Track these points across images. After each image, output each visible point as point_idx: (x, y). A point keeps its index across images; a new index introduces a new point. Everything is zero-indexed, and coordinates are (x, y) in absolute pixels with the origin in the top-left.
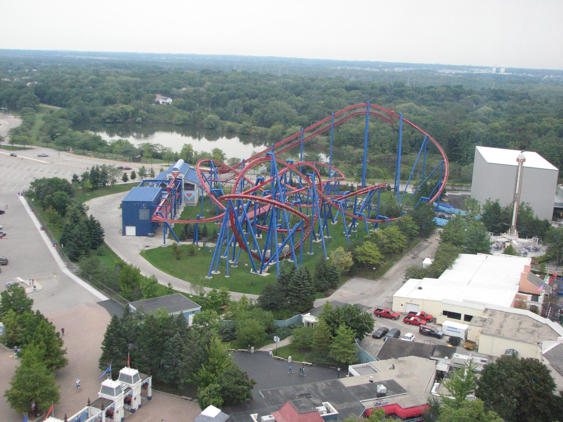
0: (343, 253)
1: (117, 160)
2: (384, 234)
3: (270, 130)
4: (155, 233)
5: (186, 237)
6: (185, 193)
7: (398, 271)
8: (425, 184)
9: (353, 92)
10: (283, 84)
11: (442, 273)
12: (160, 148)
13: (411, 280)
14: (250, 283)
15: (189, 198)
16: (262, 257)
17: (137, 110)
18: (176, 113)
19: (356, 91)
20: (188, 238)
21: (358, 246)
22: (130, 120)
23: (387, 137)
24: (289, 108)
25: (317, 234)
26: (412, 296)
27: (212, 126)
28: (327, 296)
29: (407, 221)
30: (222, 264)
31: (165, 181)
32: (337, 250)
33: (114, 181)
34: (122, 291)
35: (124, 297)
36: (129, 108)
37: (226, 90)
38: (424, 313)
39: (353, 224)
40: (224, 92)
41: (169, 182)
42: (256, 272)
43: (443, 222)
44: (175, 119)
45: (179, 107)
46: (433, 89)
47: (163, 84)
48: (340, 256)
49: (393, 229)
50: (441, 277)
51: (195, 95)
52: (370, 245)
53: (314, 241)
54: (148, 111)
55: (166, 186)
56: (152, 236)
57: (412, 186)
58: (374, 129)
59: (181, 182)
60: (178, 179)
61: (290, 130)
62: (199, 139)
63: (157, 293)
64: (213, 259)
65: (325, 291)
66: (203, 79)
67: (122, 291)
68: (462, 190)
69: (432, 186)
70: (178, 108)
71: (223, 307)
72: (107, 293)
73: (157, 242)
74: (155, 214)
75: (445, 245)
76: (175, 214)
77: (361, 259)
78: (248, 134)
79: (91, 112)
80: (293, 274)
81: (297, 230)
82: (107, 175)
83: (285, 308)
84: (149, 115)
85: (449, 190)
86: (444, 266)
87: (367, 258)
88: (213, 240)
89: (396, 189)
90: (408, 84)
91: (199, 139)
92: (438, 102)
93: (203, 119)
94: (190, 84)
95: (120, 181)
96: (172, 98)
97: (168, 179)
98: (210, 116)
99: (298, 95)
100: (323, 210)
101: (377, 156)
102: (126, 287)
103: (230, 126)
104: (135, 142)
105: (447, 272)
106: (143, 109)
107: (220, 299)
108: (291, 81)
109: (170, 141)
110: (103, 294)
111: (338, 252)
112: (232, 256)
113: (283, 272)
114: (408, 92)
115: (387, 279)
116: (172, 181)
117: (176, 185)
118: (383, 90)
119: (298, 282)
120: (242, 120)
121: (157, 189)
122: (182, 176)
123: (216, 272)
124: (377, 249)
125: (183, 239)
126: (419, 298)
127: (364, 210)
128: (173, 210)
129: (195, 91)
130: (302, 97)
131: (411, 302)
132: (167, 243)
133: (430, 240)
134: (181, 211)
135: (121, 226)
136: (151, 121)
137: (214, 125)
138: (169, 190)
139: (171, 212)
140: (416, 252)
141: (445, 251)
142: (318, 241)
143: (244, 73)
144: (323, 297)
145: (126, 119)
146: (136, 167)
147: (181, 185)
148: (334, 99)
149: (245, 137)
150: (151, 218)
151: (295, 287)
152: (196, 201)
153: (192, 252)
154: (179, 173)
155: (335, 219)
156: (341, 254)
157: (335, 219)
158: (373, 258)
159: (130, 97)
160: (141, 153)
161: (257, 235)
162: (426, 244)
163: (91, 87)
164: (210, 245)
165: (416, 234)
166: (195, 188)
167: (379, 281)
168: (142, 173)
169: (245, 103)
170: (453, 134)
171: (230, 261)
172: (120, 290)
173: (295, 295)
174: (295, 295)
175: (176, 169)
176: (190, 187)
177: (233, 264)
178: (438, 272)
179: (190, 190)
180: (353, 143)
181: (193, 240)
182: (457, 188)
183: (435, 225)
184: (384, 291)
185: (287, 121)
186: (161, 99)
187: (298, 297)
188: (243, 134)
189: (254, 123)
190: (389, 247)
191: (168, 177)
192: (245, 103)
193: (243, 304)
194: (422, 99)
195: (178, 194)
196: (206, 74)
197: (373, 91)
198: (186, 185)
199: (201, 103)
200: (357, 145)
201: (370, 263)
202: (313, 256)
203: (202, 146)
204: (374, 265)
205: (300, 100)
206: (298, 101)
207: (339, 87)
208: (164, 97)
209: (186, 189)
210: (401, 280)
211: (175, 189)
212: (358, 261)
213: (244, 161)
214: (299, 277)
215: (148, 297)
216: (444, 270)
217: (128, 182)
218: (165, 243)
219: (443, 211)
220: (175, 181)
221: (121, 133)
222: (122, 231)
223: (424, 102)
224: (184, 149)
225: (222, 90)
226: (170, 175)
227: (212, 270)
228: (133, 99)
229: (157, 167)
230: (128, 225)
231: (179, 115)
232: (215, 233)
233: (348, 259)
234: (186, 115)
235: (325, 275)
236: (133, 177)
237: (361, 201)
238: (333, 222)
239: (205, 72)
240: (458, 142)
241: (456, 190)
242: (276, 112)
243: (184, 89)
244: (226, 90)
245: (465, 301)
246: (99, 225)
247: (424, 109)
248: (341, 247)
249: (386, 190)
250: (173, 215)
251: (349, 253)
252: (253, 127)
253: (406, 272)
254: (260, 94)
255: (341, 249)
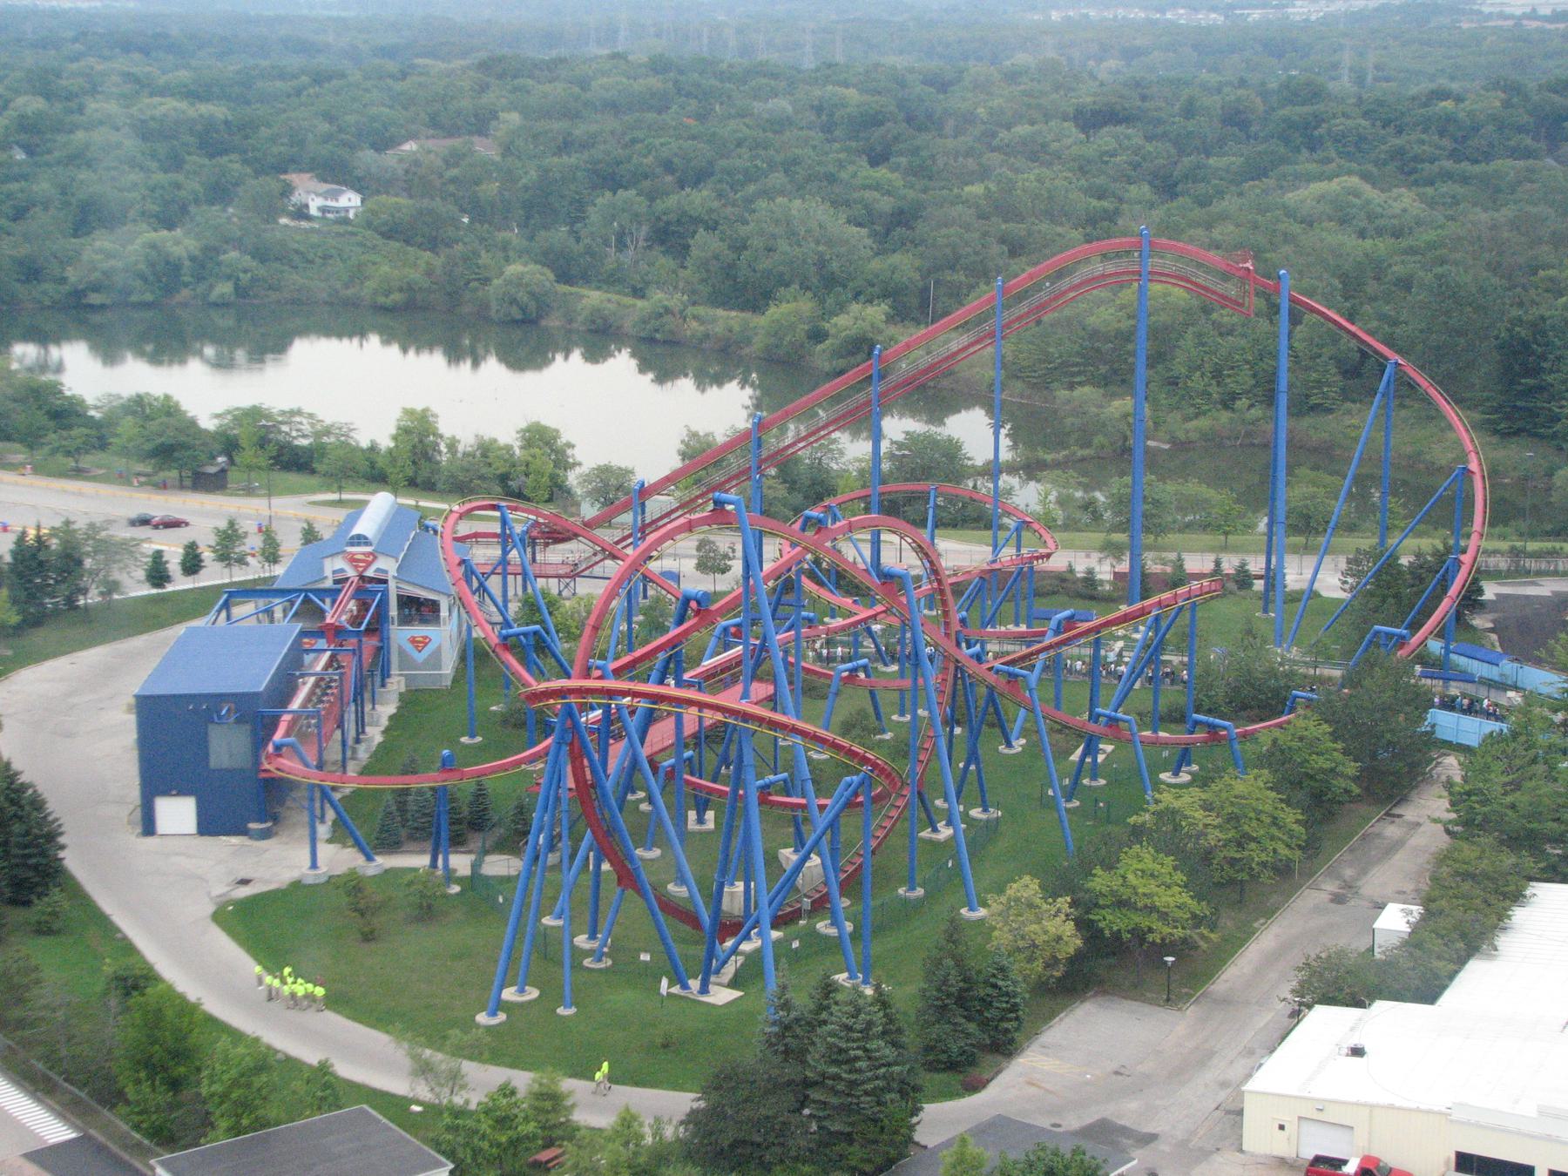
0: (1038, 901)
1: (130, 484)
2: (1207, 807)
3: (761, 321)
4: (275, 819)
5: (403, 832)
6: (400, 635)
7: (1270, 959)
8: (1391, 562)
9: (1106, 138)
10: (819, 110)
11: (1452, 976)
12: (307, 428)
13: (1320, 1010)
14: (659, 1041)
15: (420, 657)
16: (706, 918)
17: (211, 252)
18: (374, 258)
19: (1120, 129)
20: (411, 838)
21: (1098, 871)
22: (185, 293)
23: (1243, 342)
24: (837, 224)
25: (939, 803)
26: (1321, 1090)
27: (523, 309)
28: (974, 1087)
29: (1312, 745)
30: (546, 956)
31: (317, 592)
32: (1013, 890)
33: (113, 587)
34: (127, 1102)
35: (137, 1127)
36: (181, 243)
37: (584, 146)
38: (1376, 1161)
39: (1091, 750)
40: (572, 160)
41: (333, 593)
42: (685, 987)
43: (1471, 730)
44: (370, 285)
45: (390, 233)
46: (1448, 105)
47: (325, 127)
48: (1020, 917)
49: (1250, 787)
50: (1448, 998)
51: (455, 172)
52: (1149, 864)
53: (926, 834)
54: (261, 255)
55: (321, 613)
56: (265, 835)
57: (1343, 565)
58: (1187, 311)
59: (385, 593)
60: (371, 580)
61: (842, 320)
62: (476, 364)
63: (272, 1113)
64: (509, 929)
65: (963, 1068)
66: (488, 98)
67: (127, 1102)
68: (1556, 573)
69: (1420, 572)
70: (383, 234)
71: (544, 1156)
72: (68, 1110)
73: (285, 860)
74: (270, 748)
75: (1468, 851)
76: (361, 724)
77: (1111, 921)
78: (673, 343)
79: (21, 263)
80: (824, 1015)
81: (850, 804)
82: (80, 563)
83: (796, 1159)
84: (262, 272)
85: (1496, 575)
86: (1460, 945)
87: (1137, 919)
88: (511, 843)
89: (1272, 577)
90: (1344, 84)
91: (476, 364)
92: (1465, 166)
93: (486, 281)
94: (434, 123)
95: (137, 588)
96: (358, 191)
97: (329, 584)
98: (514, 269)
99: (875, 162)
100: (960, 700)
101: (1203, 423)
102: (146, 1087)
103: (596, 311)
104: (203, 391)
105: (1475, 970)
106: (238, 244)
107: (531, 1127)
108: (852, 94)
109: (348, 384)
110: (51, 1109)
111: (1017, 900)
112: (587, 917)
113: (786, 1006)
114: (1339, 124)
115: (1225, 1001)
116: (348, 591)
117: (364, 606)
118: (1236, 119)
119: (841, 1051)
120: (647, 283)
121: (287, 629)
122: (387, 565)
123: (522, 991)
124: (1180, 877)
125: (389, 843)
126: (1354, 1100)
127: (1137, 686)
128: (350, 717)
129: (453, 159)
130: (893, 170)
131: (1318, 1115)
132: (323, 868)
133: (1409, 813)
134: (386, 709)
135: (134, 794)
136: (274, 296)
137: (532, 305)
138: (336, 632)
139: (340, 725)
140: (1348, 872)
141: (1466, 876)
142: (945, 832)
143: (659, 66)
144: (959, 1095)
145: (169, 290)
146: (204, 513)
147: (383, 604)
148: (1030, 178)
149: (663, 354)
150: (257, 762)
151: (833, 1070)
152: (448, 667)
153: (427, 906)
154: (374, 556)
155: (1017, 727)
156: (1031, 906)
157: (1017, 727)
158: (1164, 916)
159: (183, 193)
160: (230, 446)
161: (692, 815)
162: (1392, 831)
163: (20, 156)
164: (499, 865)
165: (1347, 791)
166: (444, 613)
167: (1192, 1011)
168: (228, 544)
169: (660, 205)
170: (1520, 321)
171: (581, 940)
172: (121, 1095)
173: (835, 1101)
174: (835, 1101)
175: (360, 540)
176: (419, 609)
177: (590, 953)
178: (1436, 977)
179: (424, 621)
180: (1103, 369)
181: (429, 845)
182: (1531, 564)
183: (1434, 744)
184: (1211, 1054)
185: (831, 283)
186: (313, 197)
187: (846, 1109)
188: (651, 340)
189: (694, 292)
190: (1233, 862)
191: (328, 572)
192: (660, 205)
193: (627, 1144)
194: (1398, 154)
195: (370, 643)
196: (501, 76)
197: (1191, 125)
198: (407, 602)
199: (479, 211)
200: (1116, 379)
201: (1150, 937)
202: (920, 902)
203: (480, 402)
204: (1166, 947)
205: (886, 184)
206: (877, 187)
207: (1047, 117)
208: (326, 187)
209: (405, 620)
210: (1284, 1009)
211: (368, 618)
212: (1101, 931)
213: (645, 492)
214: (849, 1029)
215: (236, 1130)
216: (1462, 962)
217: (170, 588)
218: (314, 865)
219: (1467, 678)
220: (359, 590)
221: (149, 348)
222: (138, 814)
223: (1407, 168)
224: (404, 432)
225: (566, 146)
226: (340, 563)
227: (502, 987)
228: (197, 201)
229: (291, 510)
230: (166, 793)
231: (386, 268)
232: (522, 814)
233: (1058, 928)
234: (417, 267)
235: (961, 1000)
236: (192, 564)
237: (1120, 649)
238: (1009, 745)
239: (499, 69)
240: (1543, 357)
241: (1528, 573)
242: (783, 245)
243: (410, 146)
244: (584, 146)
245: (1542, 1112)
246: (38, 804)
247: (1404, 201)
248: (1027, 878)
249: (1231, 586)
250: (352, 734)
251: (1063, 902)
252: (691, 310)
253: (1302, 975)
254: (723, 163)
255: (1027, 887)
